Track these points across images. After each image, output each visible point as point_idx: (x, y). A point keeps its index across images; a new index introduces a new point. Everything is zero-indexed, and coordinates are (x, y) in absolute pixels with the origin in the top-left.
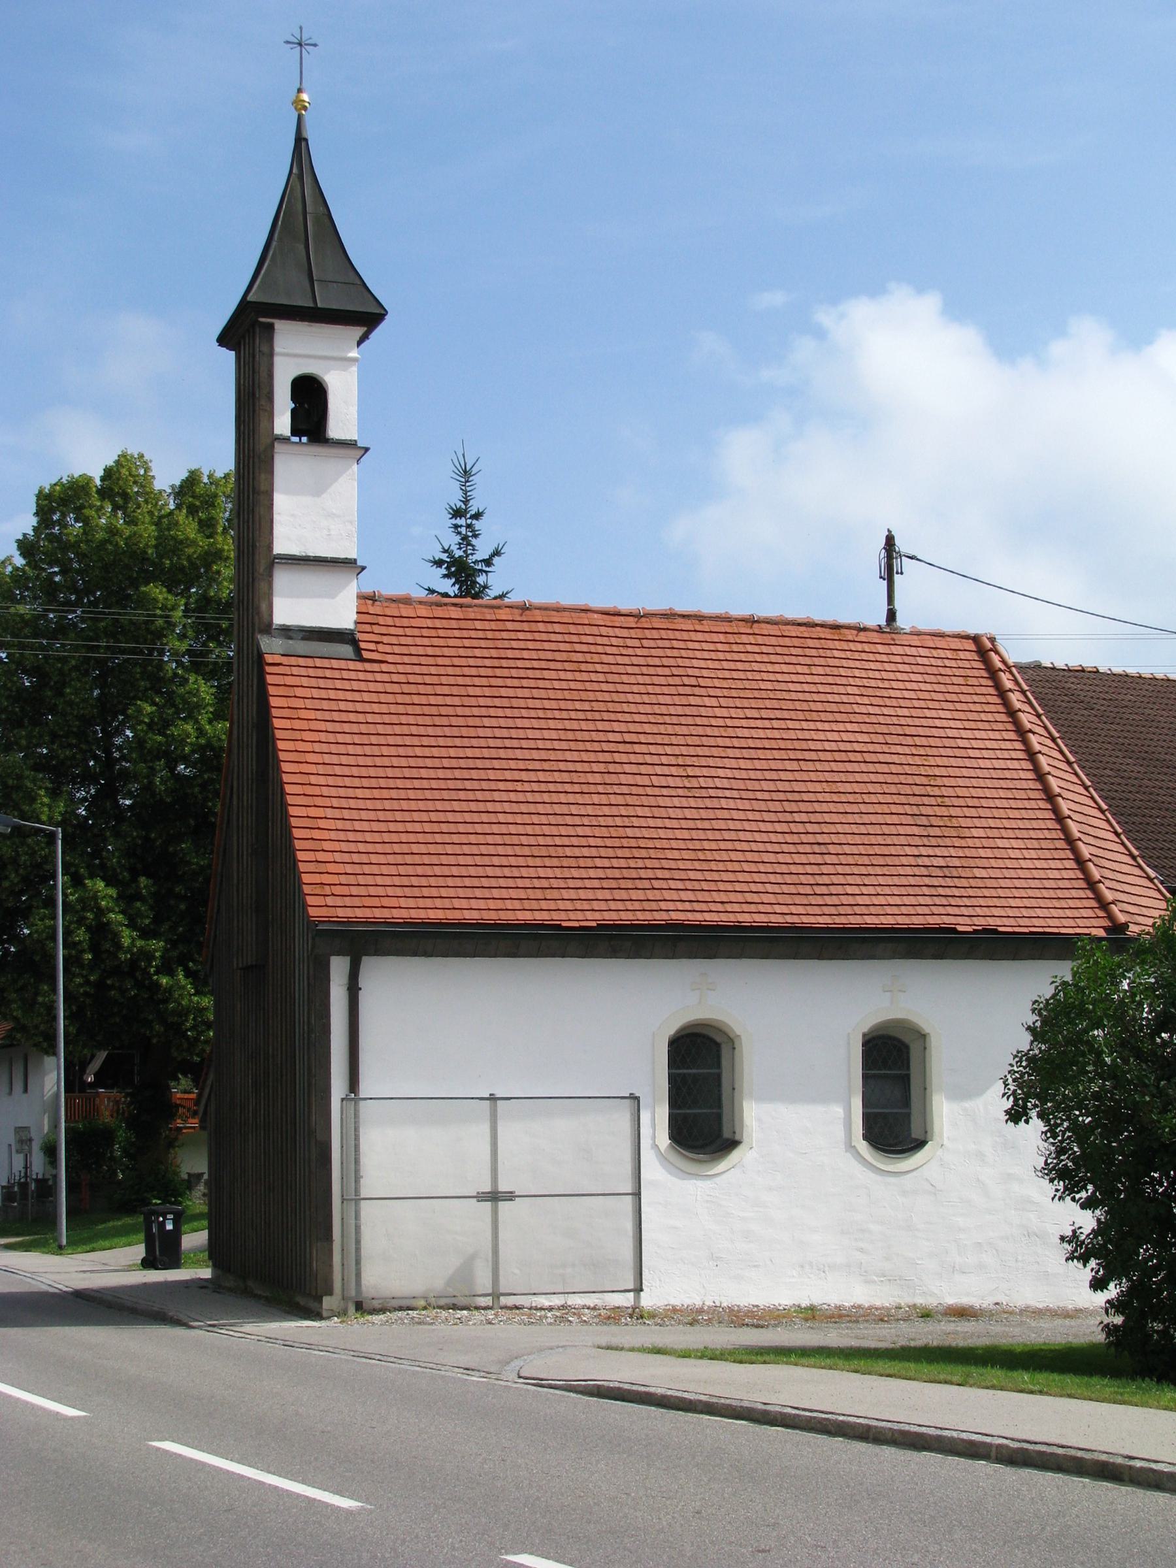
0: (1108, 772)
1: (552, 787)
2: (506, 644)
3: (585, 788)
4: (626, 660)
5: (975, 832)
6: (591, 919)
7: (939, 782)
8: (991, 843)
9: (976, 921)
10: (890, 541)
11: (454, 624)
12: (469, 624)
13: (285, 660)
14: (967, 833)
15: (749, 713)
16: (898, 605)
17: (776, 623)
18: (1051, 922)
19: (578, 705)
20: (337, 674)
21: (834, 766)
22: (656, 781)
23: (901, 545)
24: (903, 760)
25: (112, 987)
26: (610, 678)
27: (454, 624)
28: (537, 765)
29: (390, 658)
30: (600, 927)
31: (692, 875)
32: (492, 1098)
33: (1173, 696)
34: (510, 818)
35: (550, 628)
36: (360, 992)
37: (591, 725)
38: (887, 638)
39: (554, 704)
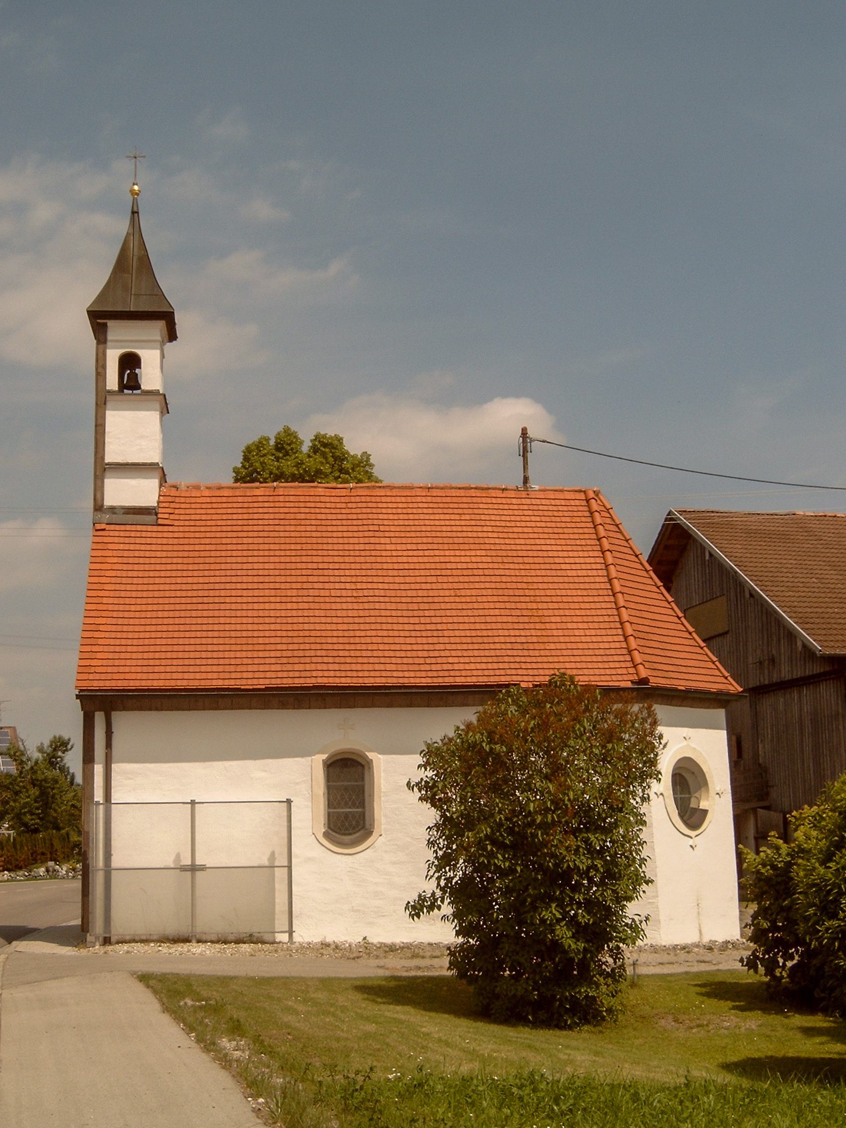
0: (814, 580)
1: (261, 600)
2: (255, 510)
3: (284, 599)
4: (334, 517)
5: (553, 619)
6: (262, 683)
7: (535, 586)
8: (564, 626)
9: (537, 678)
10: (524, 432)
11: (224, 500)
12: (235, 499)
13: (108, 527)
14: (547, 619)
15: (409, 547)
16: (531, 473)
17: (442, 488)
18: (592, 678)
19: (293, 547)
20: (138, 534)
21: (462, 579)
22: (333, 593)
23: (531, 433)
24: (512, 573)
25: (599, 783)
26: (319, 528)
27: (224, 500)
28: (255, 586)
29: (176, 523)
30: (267, 689)
31: (341, 653)
32: (193, 803)
33: (845, 524)
34: (228, 620)
35: (287, 499)
36: (113, 735)
37: (298, 559)
38: (524, 494)
39: (277, 547)
